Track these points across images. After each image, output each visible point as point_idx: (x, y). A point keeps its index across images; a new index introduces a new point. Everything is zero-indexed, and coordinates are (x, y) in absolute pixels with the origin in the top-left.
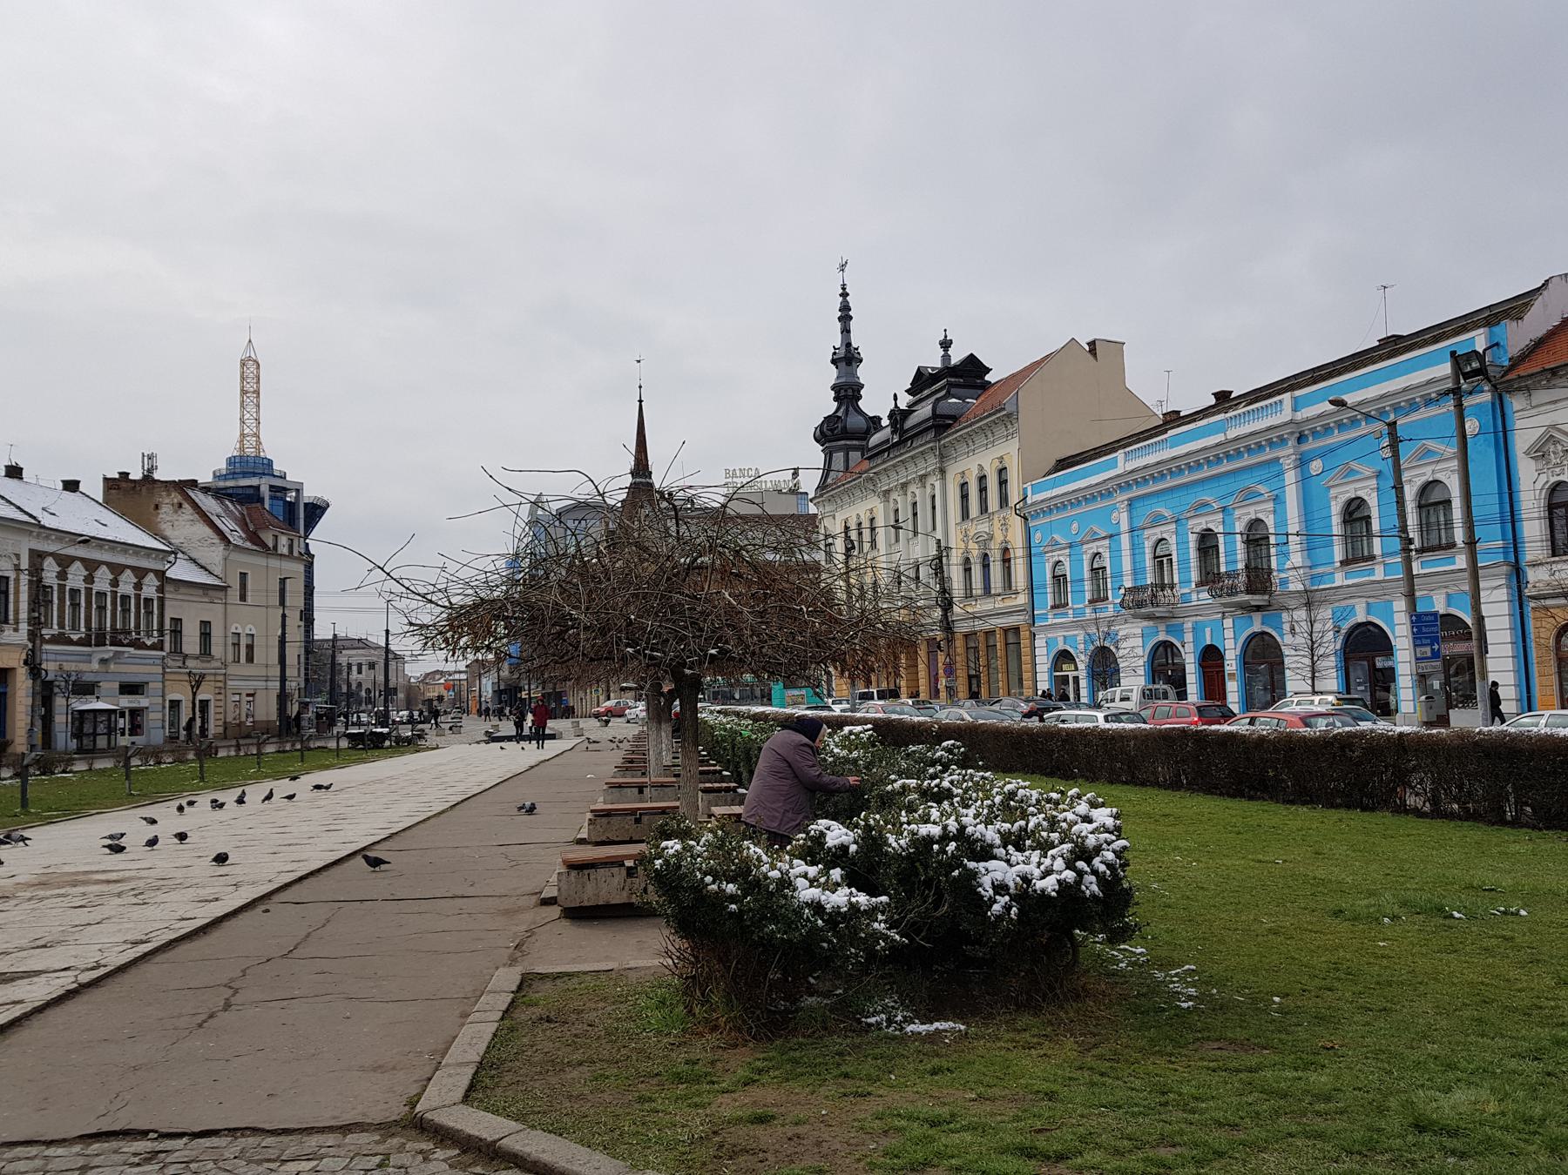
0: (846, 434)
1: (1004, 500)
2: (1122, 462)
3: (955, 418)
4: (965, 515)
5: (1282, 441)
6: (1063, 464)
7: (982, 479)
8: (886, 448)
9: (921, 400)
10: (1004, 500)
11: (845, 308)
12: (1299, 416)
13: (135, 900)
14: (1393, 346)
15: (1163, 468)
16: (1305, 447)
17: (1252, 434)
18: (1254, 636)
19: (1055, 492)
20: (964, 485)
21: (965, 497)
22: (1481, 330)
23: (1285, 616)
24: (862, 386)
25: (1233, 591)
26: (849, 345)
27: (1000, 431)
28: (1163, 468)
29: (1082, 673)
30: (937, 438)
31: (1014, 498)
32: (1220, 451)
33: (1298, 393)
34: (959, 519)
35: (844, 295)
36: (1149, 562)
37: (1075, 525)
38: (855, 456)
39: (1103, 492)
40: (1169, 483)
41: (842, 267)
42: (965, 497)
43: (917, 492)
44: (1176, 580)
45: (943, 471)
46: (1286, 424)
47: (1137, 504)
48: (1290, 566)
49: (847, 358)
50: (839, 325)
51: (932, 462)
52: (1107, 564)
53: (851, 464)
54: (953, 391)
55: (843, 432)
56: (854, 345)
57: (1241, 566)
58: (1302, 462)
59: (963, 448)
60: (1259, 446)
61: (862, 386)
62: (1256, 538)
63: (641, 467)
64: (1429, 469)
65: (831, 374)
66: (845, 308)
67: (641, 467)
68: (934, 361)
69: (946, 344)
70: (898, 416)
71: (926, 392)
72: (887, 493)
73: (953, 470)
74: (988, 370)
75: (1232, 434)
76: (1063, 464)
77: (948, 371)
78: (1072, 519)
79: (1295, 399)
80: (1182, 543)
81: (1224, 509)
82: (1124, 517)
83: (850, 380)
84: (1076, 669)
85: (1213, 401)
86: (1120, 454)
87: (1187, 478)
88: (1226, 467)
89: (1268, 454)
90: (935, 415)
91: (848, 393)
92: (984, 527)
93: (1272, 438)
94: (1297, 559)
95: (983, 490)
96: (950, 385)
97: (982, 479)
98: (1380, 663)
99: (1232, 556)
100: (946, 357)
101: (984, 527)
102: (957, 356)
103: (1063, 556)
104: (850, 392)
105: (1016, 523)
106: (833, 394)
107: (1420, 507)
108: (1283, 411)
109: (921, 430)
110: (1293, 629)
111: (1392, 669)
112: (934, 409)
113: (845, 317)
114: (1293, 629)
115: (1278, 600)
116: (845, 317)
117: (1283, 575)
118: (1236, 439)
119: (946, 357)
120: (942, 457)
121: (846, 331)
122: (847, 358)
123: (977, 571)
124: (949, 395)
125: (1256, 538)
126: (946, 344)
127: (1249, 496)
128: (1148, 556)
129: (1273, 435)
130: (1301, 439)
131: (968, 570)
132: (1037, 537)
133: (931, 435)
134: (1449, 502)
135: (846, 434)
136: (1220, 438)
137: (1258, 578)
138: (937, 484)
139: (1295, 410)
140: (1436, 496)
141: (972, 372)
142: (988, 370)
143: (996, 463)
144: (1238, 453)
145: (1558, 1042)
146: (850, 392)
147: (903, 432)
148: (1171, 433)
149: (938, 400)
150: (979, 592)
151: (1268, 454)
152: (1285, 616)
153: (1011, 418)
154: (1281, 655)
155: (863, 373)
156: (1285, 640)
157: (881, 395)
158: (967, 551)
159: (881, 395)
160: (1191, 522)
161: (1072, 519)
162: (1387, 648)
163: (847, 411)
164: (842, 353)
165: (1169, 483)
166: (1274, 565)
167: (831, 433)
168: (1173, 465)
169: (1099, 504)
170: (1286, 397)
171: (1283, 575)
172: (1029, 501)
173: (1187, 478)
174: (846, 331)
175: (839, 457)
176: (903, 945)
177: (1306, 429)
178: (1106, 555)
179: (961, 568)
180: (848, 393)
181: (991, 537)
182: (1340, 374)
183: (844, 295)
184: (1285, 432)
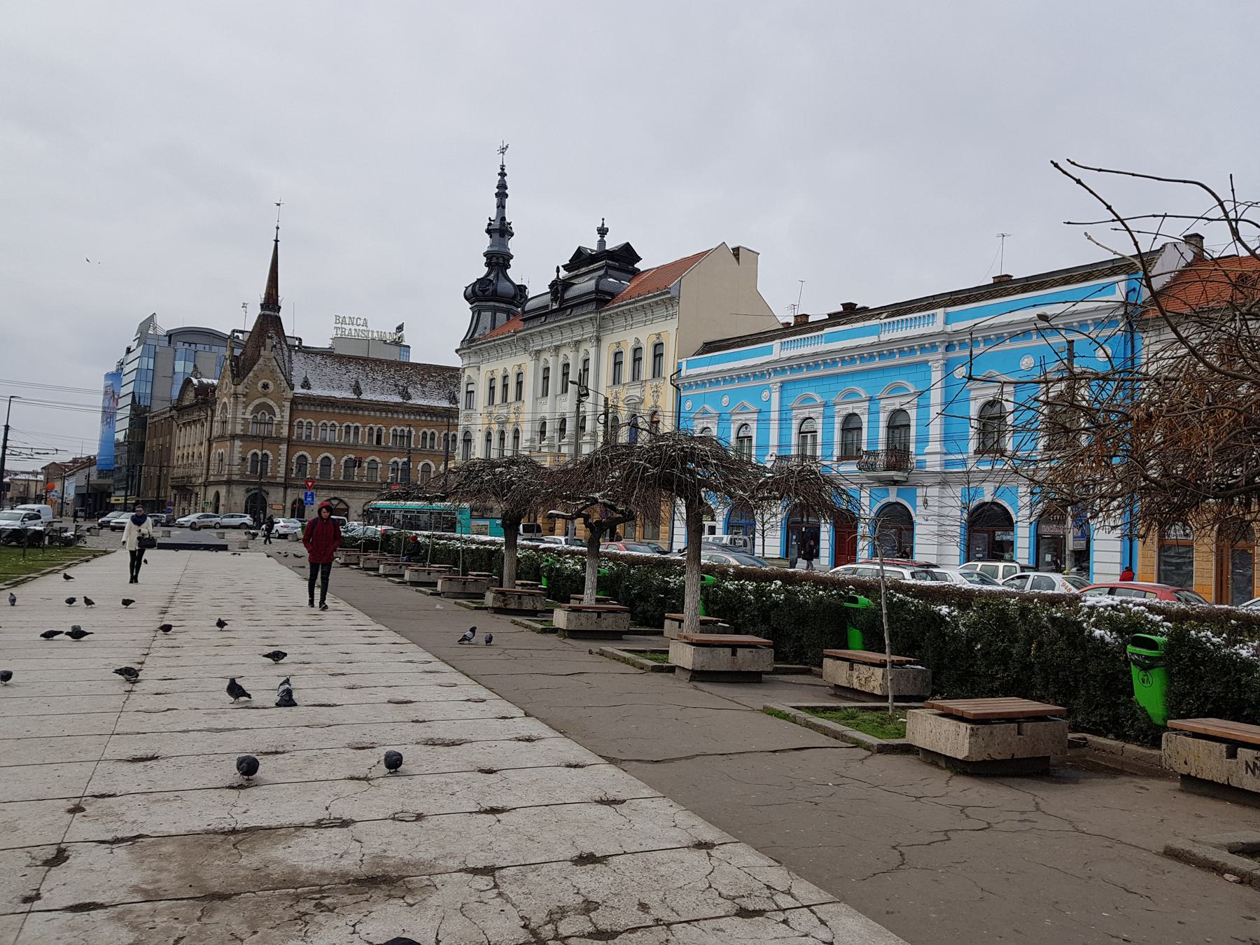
0: (496, 296)
1: (657, 372)
2: (777, 351)
3: (613, 295)
4: (616, 380)
5: (933, 347)
6: (710, 347)
7: (637, 350)
8: (542, 314)
9: (576, 276)
10: (657, 372)
11: (502, 186)
12: (949, 329)
13: (1019, 826)
14: (1003, 286)
15: (819, 359)
16: (952, 355)
17: (905, 339)
18: (889, 505)
19: (704, 370)
20: (618, 354)
21: (617, 364)
22: (1123, 277)
23: (920, 492)
24: (511, 257)
25: (872, 467)
26: (503, 219)
27: (661, 311)
28: (819, 359)
30: (598, 309)
31: (668, 368)
32: (875, 350)
33: (950, 310)
34: (610, 383)
35: (503, 174)
36: (794, 439)
37: (726, 399)
38: (501, 317)
39: (760, 373)
40: (822, 371)
41: (503, 150)
42: (617, 364)
43: (551, 360)
44: (819, 453)
45: (598, 340)
46: (939, 334)
47: (788, 387)
48: (929, 453)
49: (500, 230)
50: (495, 200)
51: (590, 330)
52: (754, 434)
53: (498, 324)
54: (610, 272)
55: (493, 295)
56: (508, 220)
57: (882, 447)
58: (948, 367)
59: (622, 322)
60: (912, 350)
61: (511, 257)
62: (897, 424)
63: (271, 301)
64: (850, 406)
65: (485, 242)
66: (502, 186)
67: (271, 301)
68: (592, 245)
69: (603, 231)
70: (559, 287)
71: (583, 270)
72: (538, 352)
74: (639, 259)
75: (885, 337)
76: (710, 347)
77: (604, 254)
78: (724, 393)
79: (947, 314)
80: (873, 423)
81: (871, 399)
82: (776, 397)
83: (502, 250)
84: (713, 520)
85: (841, 309)
86: (776, 344)
87: (840, 369)
88: (877, 363)
89: (918, 357)
90: (597, 290)
91: (498, 261)
92: (636, 392)
93: (926, 344)
94: (935, 446)
95: (637, 360)
96: (609, 266)
97: (637, 350)
98: (1000, 535)
99: (874, 436)
101: (636, 392)
102: (612, 243)
103: (816, 413)
104: (501, 261)
105: (668, 392)
107: (888, 427)
108: (936, 321)
110: (926, 502)
111: (1012, 543)
112: (597, 285)
113: (502, 194)
114: (926, 502)
115: (913, 479)
116: (502, 194)
117: (919, 458)
118: (889, 342)
120: (600, 327)
121: (501, 206)
122: (500, 230)
124: (606, 275)
125: (897, 424)
126: (603, 231)
127: (897, 390)
128: (795, 431)
129: (927, 342)
130: (949, 347)
131: (489, 440)
132: (687, 406)
133: (592, 307)
134: (861, 429)
135: (496, 296)
136: (874, 339)
137: (898, 456)
138: (592, 351)
139: (946, 323)
140: (900, 421)
141: (625, 258)
142: (639, 259)
143: (654, 339)
144: (891, 353)
146: (501, 261)
147: (563, 301)
148: (827, 330)
149: (601, 277)
151: (918, 357)
152: (920, 492)
153: (673, 301)
154: (912, 523)
155: (513, 245)
156: (918, 514)
157: (534, 272)
159: (534, 272)
160: (882, 402)
161: (724, 393)
162: (1008, 523)
163: (497, 277)
164: (496, 225)
165: (822, 371)
166: (912, 448)
167: (480, 294)
168: (828, 358)
169: (752, 383)
170: (940, 312)
171: (919, 458)
172: (683, 374)
173: (840, 369)
174: (501, 206)
175: (486, 317)
177: (955, 340)
178: (754, 426)
180: (498, 261)
181: (642, 401)
182: (978, 300)
183: (503, 174)
184: (937, 340)
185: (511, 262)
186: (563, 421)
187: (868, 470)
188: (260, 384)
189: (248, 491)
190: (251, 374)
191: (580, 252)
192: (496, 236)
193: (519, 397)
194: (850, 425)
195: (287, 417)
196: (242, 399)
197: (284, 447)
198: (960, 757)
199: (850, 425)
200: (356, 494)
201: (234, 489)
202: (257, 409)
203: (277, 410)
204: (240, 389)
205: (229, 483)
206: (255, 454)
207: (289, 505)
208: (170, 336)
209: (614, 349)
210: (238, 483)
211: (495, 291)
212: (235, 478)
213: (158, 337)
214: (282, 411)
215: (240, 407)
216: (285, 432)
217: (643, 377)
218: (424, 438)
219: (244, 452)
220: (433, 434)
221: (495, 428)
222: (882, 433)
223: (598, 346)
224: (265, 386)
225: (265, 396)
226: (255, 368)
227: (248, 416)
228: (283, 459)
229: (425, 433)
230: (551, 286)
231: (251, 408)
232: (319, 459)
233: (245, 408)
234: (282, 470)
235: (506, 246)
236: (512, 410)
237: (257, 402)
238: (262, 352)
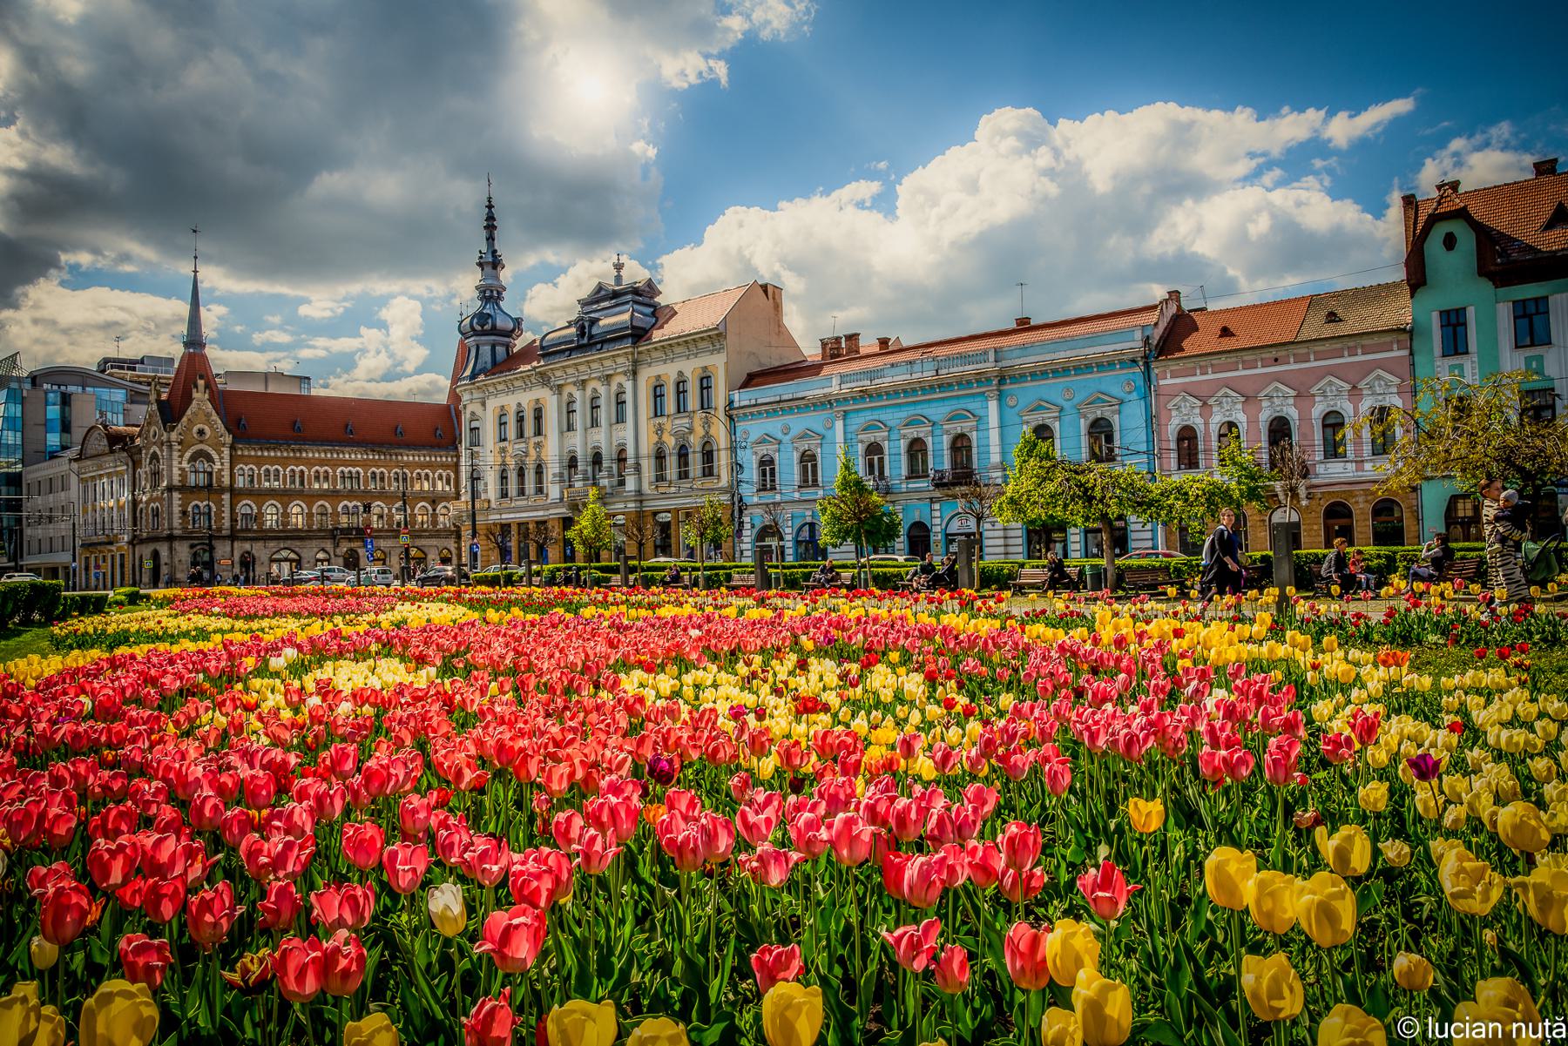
1: (705, 405)
10: (705, 405)
11: (491, 218)
29: (789, 544)
35: (490, 207)
45: (635, 373)
62: (960, 445)
66: (491, 218)
67: (194, 341)
68: (610, 282)
73: (647, 374)
84: (781, 539)
100: (618, 278)
106: (477, 293)
109: (613, 338)
119: (618, 278)
121: (491, 239)
123: (530, 477)
125: (960, 445)
138: (628, 386)
145: (1564, 616)
147: (591, 337)
150: (699, 472)
158: (504, 464)
174: (491, 239)
176: (1533, 524)
179: (653, 461)
183: (490, 207)
186: (622, 451)
187: (374, 986)
188: (195, 429)
189: (192, 546)
190: (185, 419)
191: (600, 288)
192: (488, 269)
193: (538, 432)
194: (916, 449)
195: (227, 465)
197: (226, 497)
199: (916, 449)
200: (307, 543)
201: (176, 544)
202: (193, 459)
203: (216, 457)
204: (174, 436)
205: (171, 538)
206: (197, 506)
207: (237, 558)
208: (34, 379)
209: (653, 382)
210: (182, 538)
211: (494, 326)
212: (177, 532)
213: (19, 380)
215: (176, 454)
216: (226, 481)
217: (690, 408)
219: (184, 506)
220: (302, 472)
221: (511, 463)
222: (947, 454)
223: (635, 380)
224: (201, 432)
226: (189, 412)
227: (185, 465)
228: (227, 509)
229: (268, 470)
231: (188, 455)
234: (227, 523)
235: (497, 278)
236: (531, 445)
238: (195, 395)
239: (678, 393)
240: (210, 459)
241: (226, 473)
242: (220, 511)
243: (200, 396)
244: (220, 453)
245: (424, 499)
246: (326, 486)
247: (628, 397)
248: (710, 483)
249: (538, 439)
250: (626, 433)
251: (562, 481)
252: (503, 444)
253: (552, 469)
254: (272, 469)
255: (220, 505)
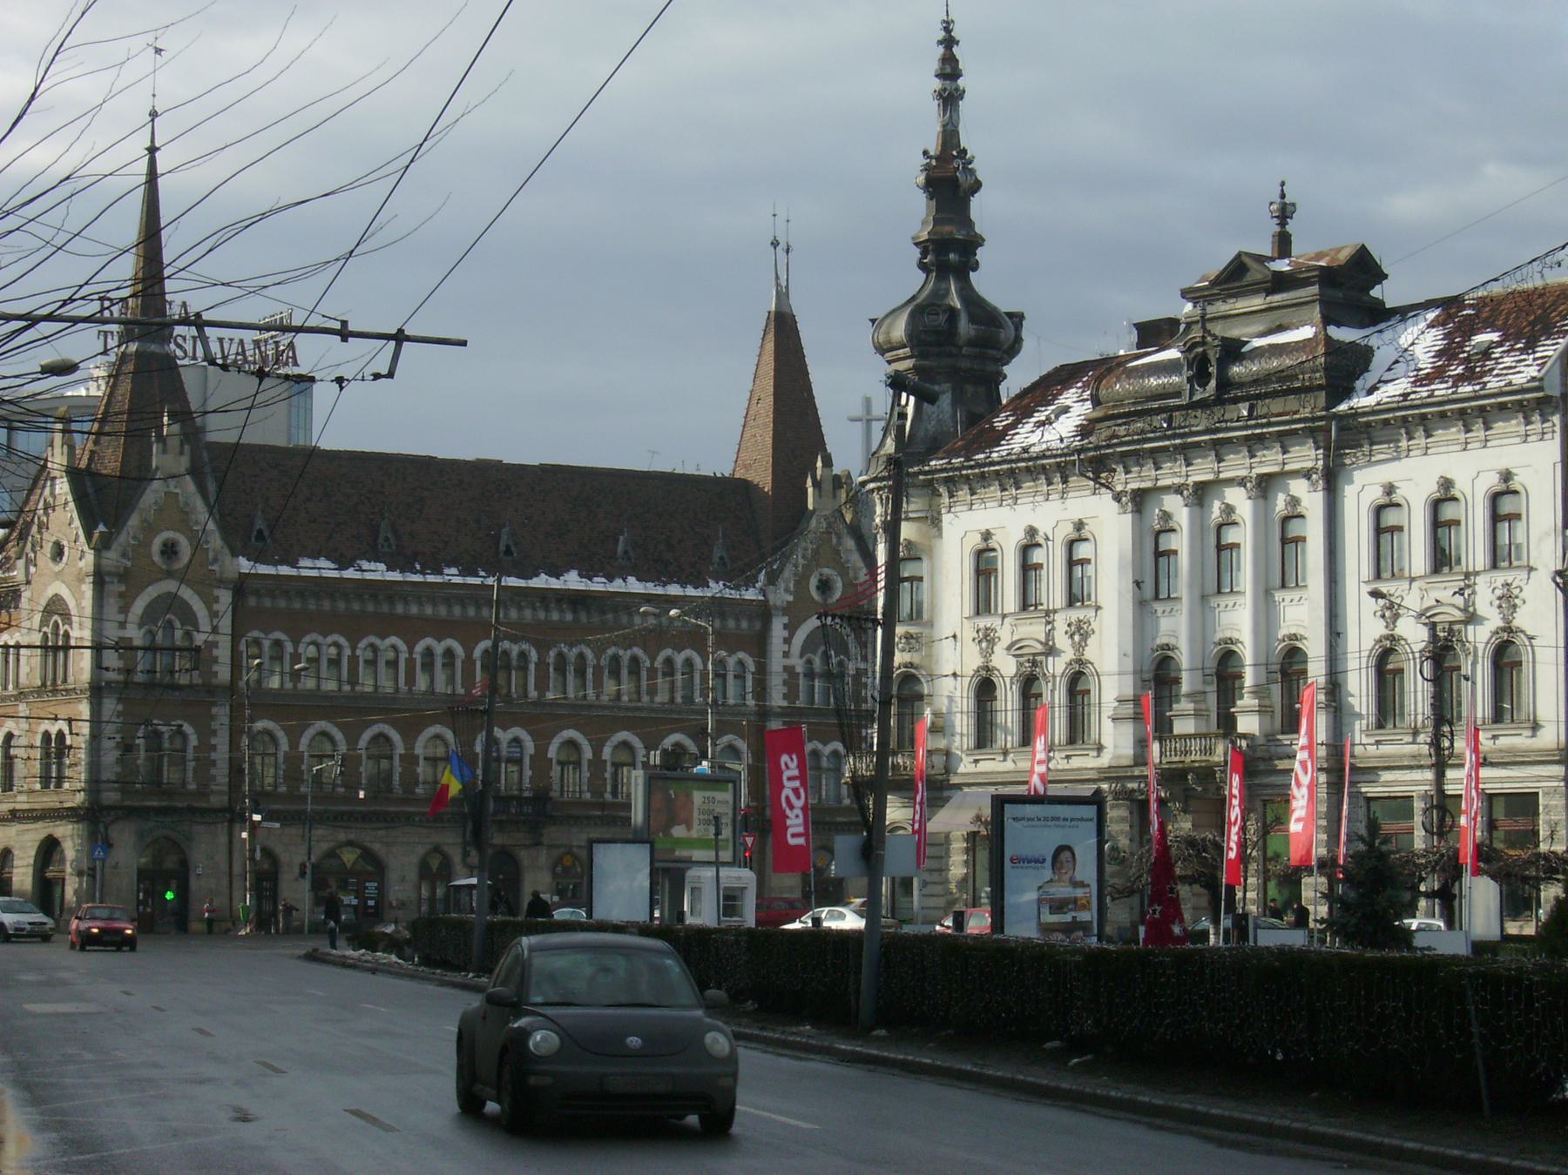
35: (949, 42)
73: (1363, 486)
74: (1380, 276)
100: (1283, 244)
102: (1315, 243)
119: (1283, 244)
143: (1491, 481)
147: (1225, 384)
154: (745, 481)
183: (949, 42)
185: (981, 254)
196: (115, 587)
197: (222, 713)
198: (617, 848)
203: (198, 606)
214: (214, 615)
218: (721, 676)
220: (689, 663)
221: (1006, 666)
224: (170, 550)
225: (169, 574)
228: (222, 742)
229: (561, 657)
230: (922, 266)
231: (139, 606)
232: (363, 741)
233: (125, 610)
237: (152, 592)
239: (1379, 531)
240: (189, 617)
241: (223, 653)
242: (206, 746)
243: (166, 459)
244: (209, 601)
245: (629, 724)
246: (330, 686)
247: (1314, 531)
248: (1514, 740)
249: (1075, 614)
250: (1301, 615)
251: (1137, 718)
252: (984, 622)
253: (1112, 683)
254: (439, 648)
255: (206, 733)
